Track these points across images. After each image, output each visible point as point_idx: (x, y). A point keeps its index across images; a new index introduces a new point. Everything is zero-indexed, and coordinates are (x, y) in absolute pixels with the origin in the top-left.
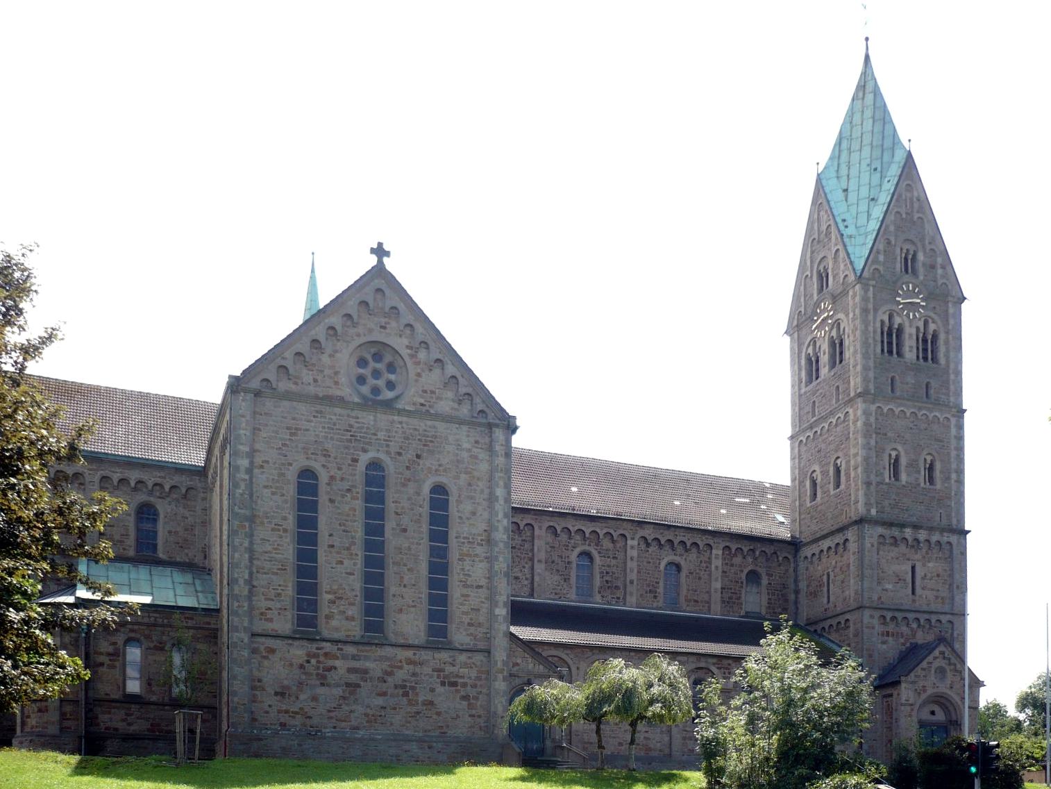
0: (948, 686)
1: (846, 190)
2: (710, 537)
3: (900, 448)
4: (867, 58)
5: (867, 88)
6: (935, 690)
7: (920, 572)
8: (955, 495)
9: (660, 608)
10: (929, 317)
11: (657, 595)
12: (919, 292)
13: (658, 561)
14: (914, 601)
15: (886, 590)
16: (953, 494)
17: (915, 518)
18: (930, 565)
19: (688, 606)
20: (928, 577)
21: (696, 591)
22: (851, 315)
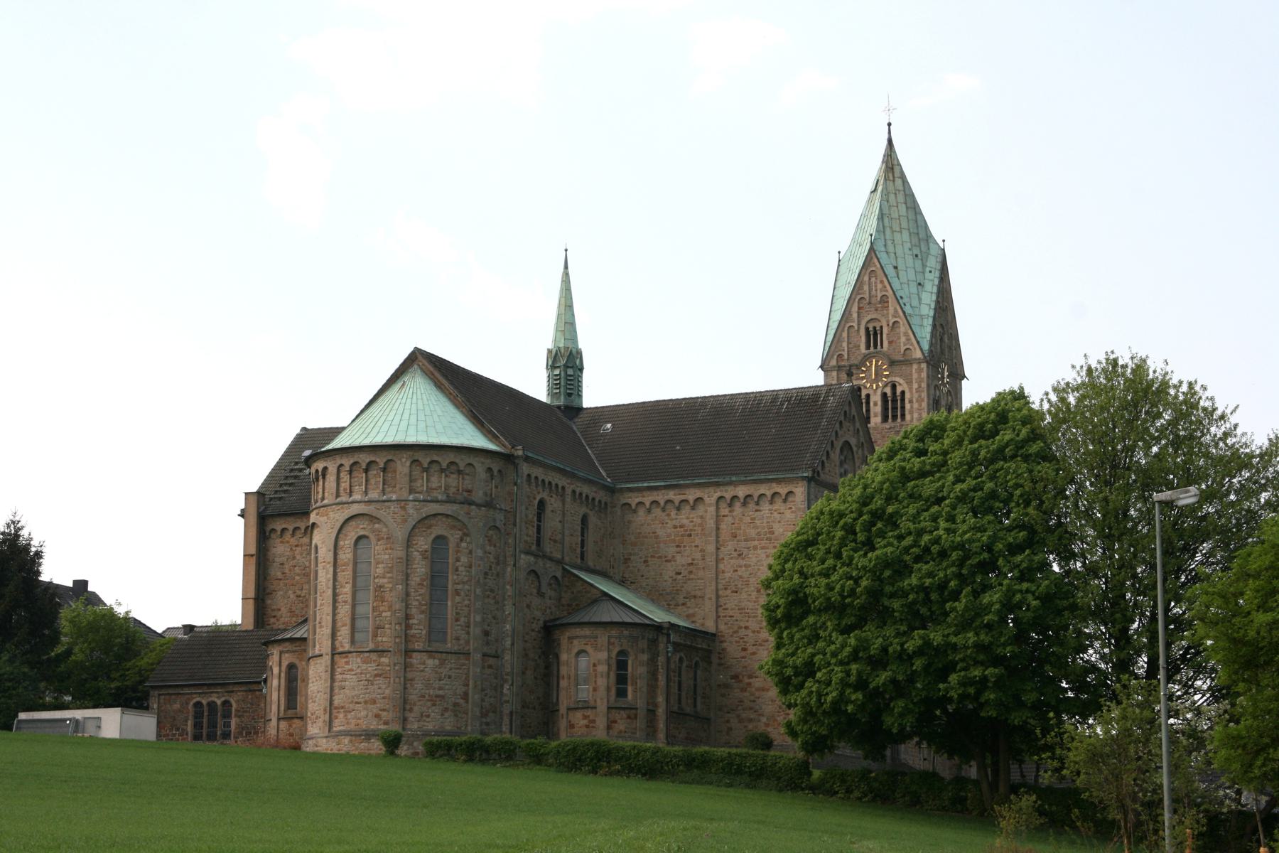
1: (896, 268)
4: (890, 141)
5: (891, 164)
22: (915, 386)
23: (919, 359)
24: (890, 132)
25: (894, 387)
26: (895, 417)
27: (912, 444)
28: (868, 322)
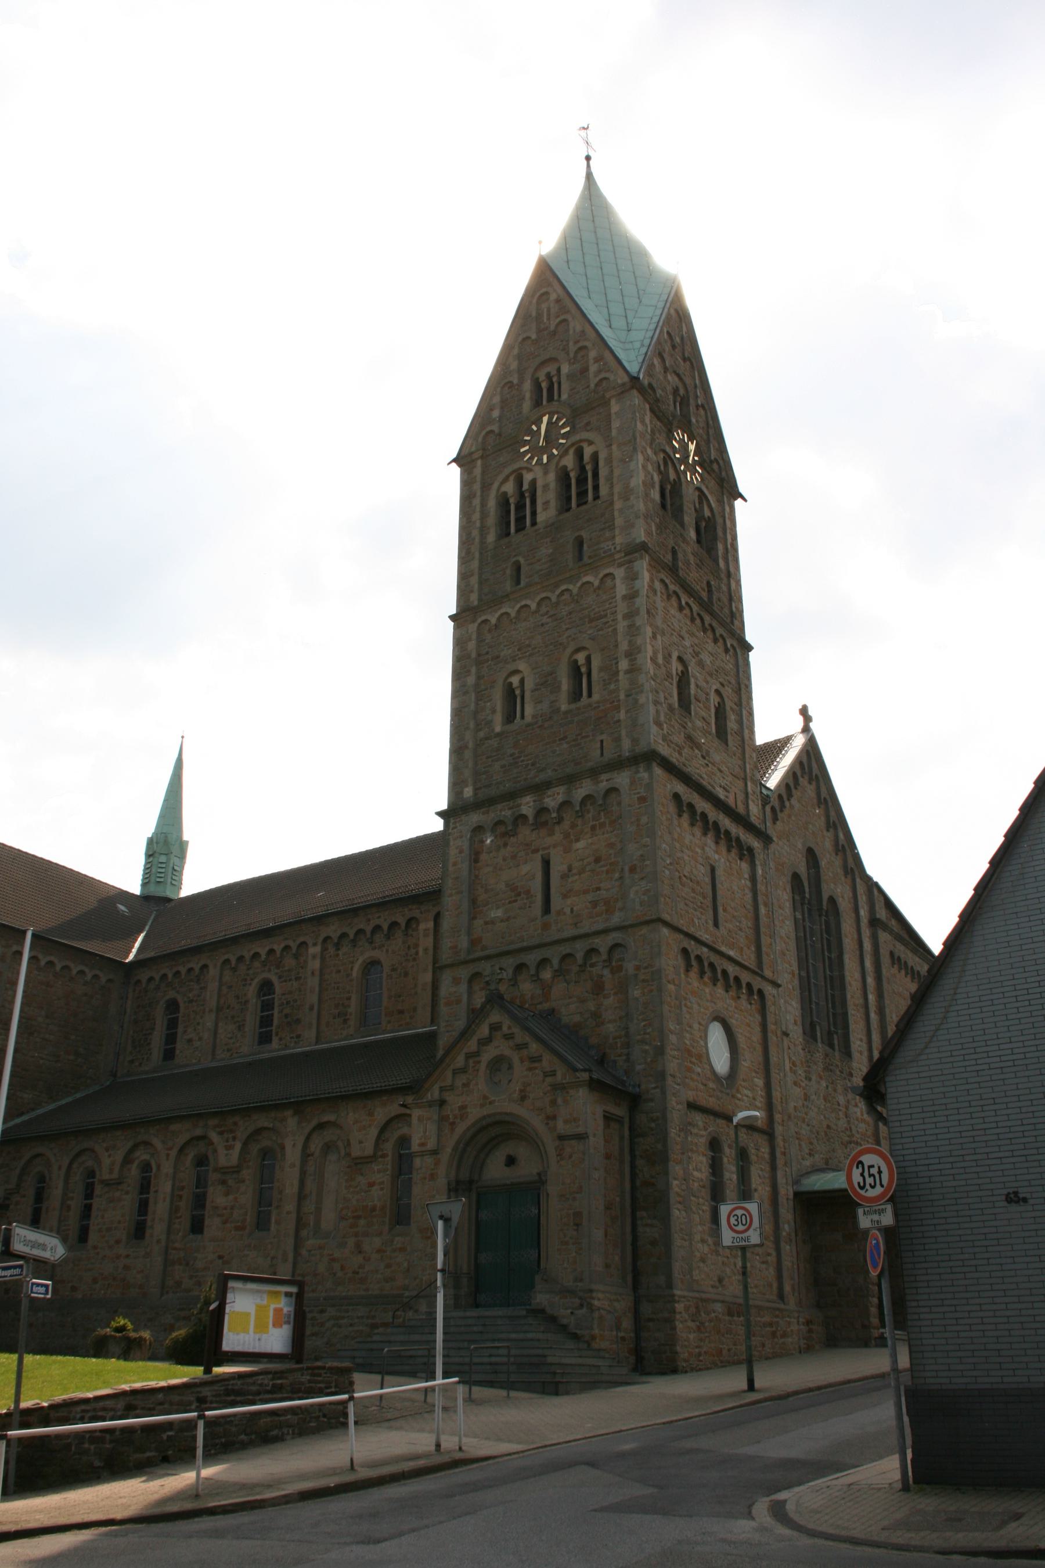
0: (516, 1096)
2: (414, 907)
3: (522, 666)
4: (589, 176)
6: (485, 1112)
7: (557, 868)
8: (627, 696)
9: (352, 1037)
10: (581, 441)
11: (348, 1017)
12: (530, 432)
13: (350, 966)
14: (546, 926)
15: (493, 922)
16: (622, 697)
17: (549, 771)
18: (581, 844)
19: (389, 1022)
20: (575, 871)
21: (400, 996)
23: (624, 384)
24: (588, 166)
25: (579, 454)
26: (520, 527)
27: (248, 982)
28: (536, 370)
